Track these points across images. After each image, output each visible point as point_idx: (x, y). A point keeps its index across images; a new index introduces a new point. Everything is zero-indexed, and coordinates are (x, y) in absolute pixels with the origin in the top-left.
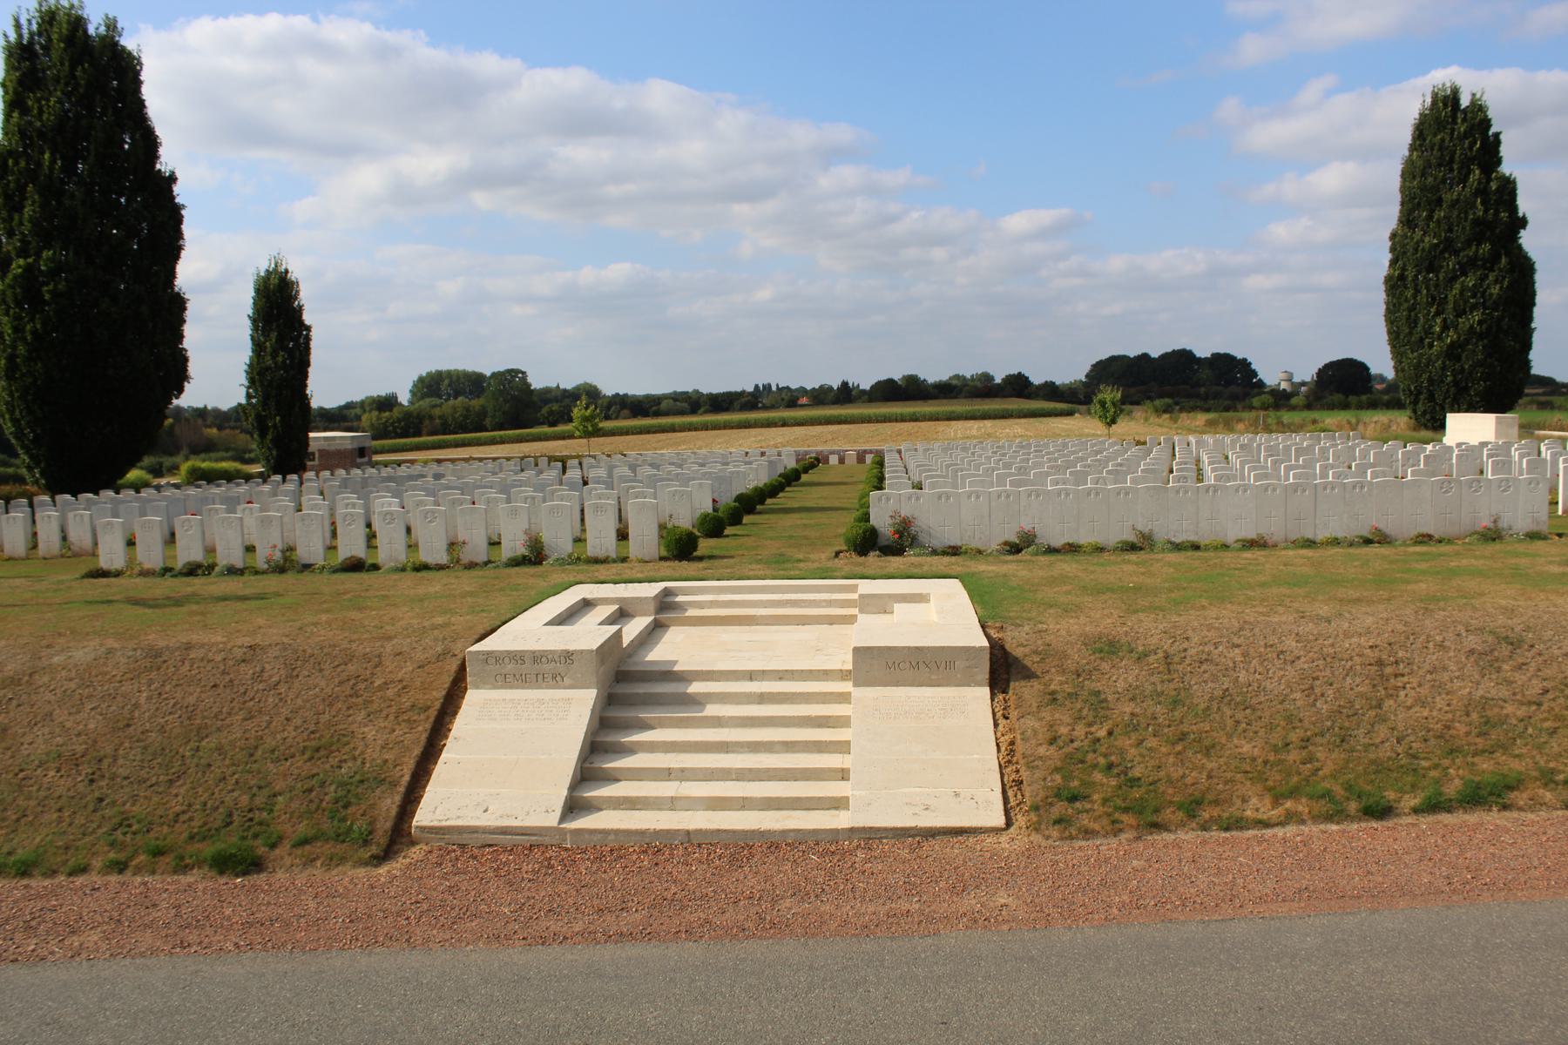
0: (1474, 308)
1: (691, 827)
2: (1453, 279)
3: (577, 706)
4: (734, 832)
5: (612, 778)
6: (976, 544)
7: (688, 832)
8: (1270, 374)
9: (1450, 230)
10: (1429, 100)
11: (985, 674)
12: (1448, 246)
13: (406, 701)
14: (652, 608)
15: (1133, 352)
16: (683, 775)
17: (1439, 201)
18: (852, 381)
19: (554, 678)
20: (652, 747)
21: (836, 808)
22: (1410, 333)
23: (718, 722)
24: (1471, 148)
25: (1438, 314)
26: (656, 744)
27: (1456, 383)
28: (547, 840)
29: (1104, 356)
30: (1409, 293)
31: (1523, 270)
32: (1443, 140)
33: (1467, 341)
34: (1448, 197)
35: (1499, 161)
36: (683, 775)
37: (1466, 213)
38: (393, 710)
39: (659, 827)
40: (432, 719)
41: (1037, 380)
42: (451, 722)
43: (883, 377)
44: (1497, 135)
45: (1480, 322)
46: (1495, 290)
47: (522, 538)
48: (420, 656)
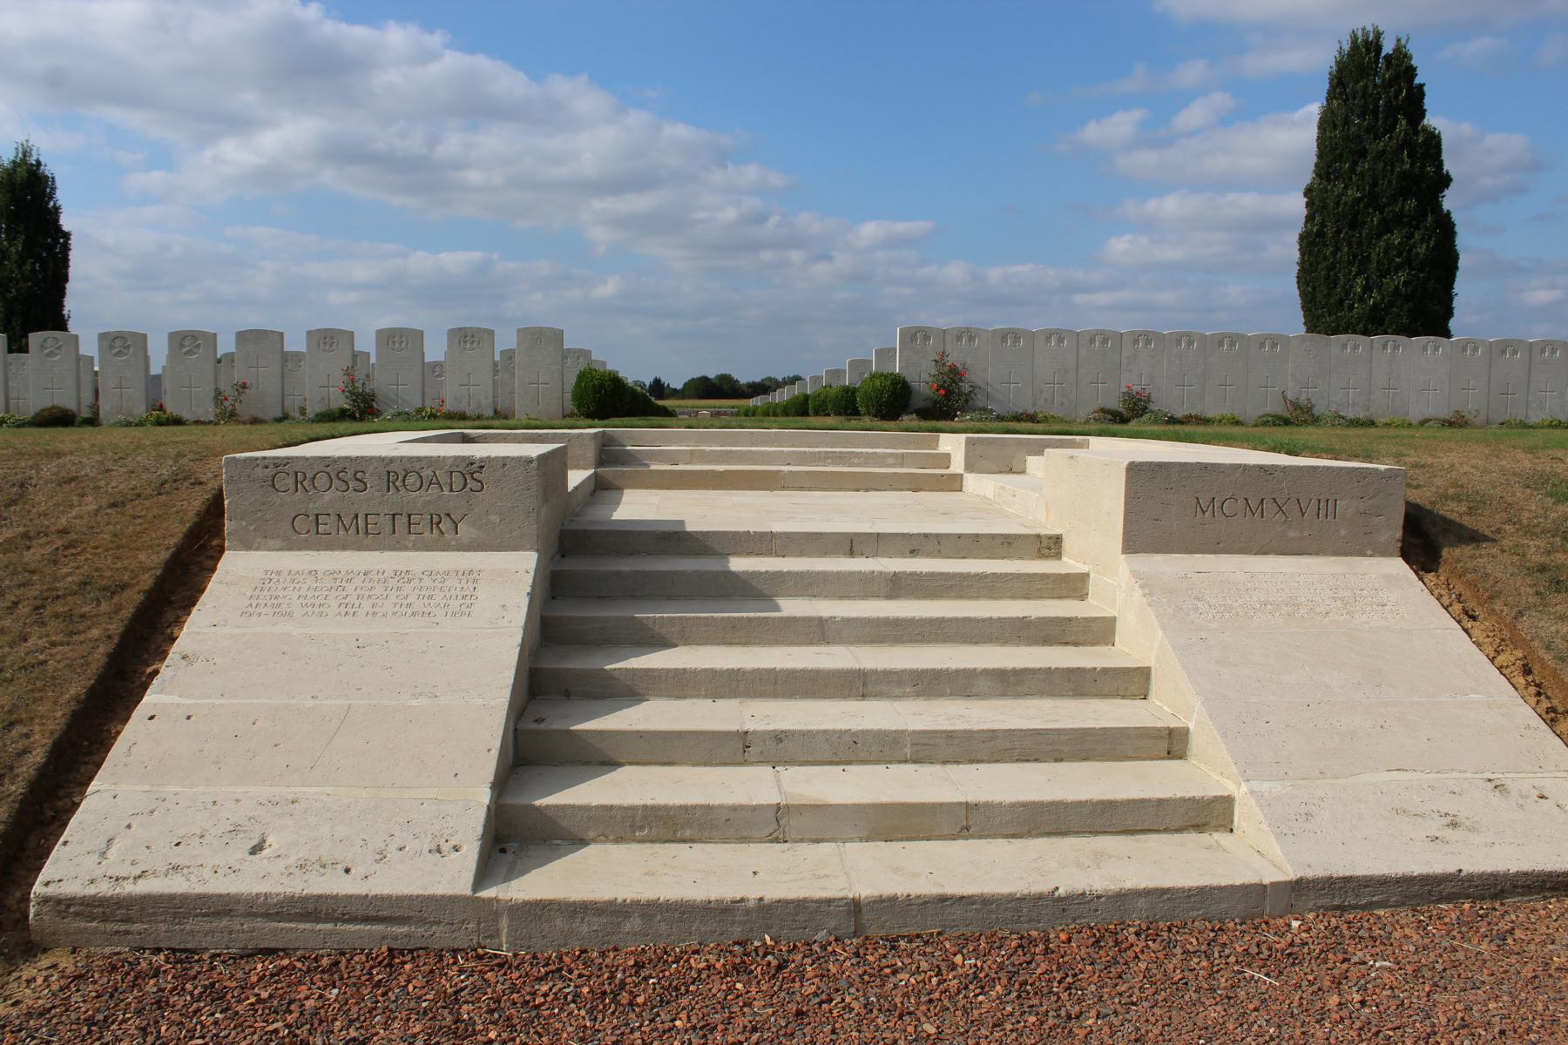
0: (1399, 267)
1: (865, 889)
3: (498, 589)
4: (985, 901)
5: (599, 757)
6: (1054, 411)
7: (855, 907)
9: (1375, 184)
10: (1347, 47)
11: (1394, 531)
13: (69, 573)
14: (590, 453)
16: (781, 749)
17: (1363, 153)
18: (665, 380)
19: (435, 523)
20: (681, 684)
21: (1199, 827)
22: (1329, 295)
23: (819, 632)
24: (1396, 97)
25: (1359, 273)
26: (680, 683)
28: (440, 936)
31: (1446, 227)
32: (1366, 87)
33: (1391, 304)
34: (1374, 147)
35: (1422, 114)
36: (781, 749)
37: (1393, 166)
38: (33, 591)
39: (775, 891)
40: (128, 612)
42: (179, 622)
43: (697, 375)
44: (1421, 86)
45: (1406, 284)
46: (1422, 249)
47: (339, 379)
48: (119, 483)
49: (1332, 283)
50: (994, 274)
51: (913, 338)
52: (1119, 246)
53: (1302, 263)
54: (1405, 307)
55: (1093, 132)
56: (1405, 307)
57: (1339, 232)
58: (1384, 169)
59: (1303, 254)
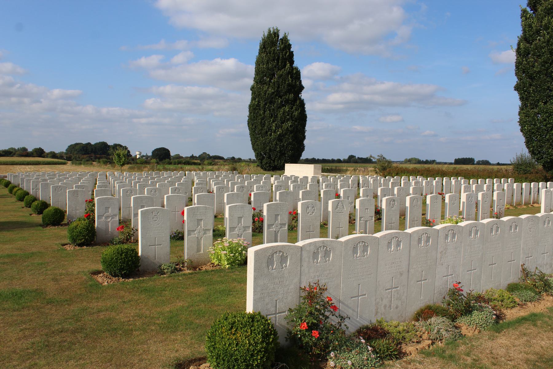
0: (288, 120)
2: (280, 108)
8: (136, 153)
9: (278, 87)
10: (266, 34)
12: (278, 94)
15: (84, 142)
20: (381, 205)
22: (262, 129)
24: (285, 55)
25: (273, 122)
27: (280, 151)
29: (73, 143)
30: (262, 112)
32: (274, 50)
33: (286, 134)
37: (285, 81)
41: (47, 150)
45: (291, 126)
49: (263, 125)
50: (104, 110)
51: (270, 262)
52: (150, 102)
53: (250, 117)
54: (291, 135)
55: (143, 61)
56: (291, 135)
57: (266, 104)
58: (282, 82)
59: (250, 113)
